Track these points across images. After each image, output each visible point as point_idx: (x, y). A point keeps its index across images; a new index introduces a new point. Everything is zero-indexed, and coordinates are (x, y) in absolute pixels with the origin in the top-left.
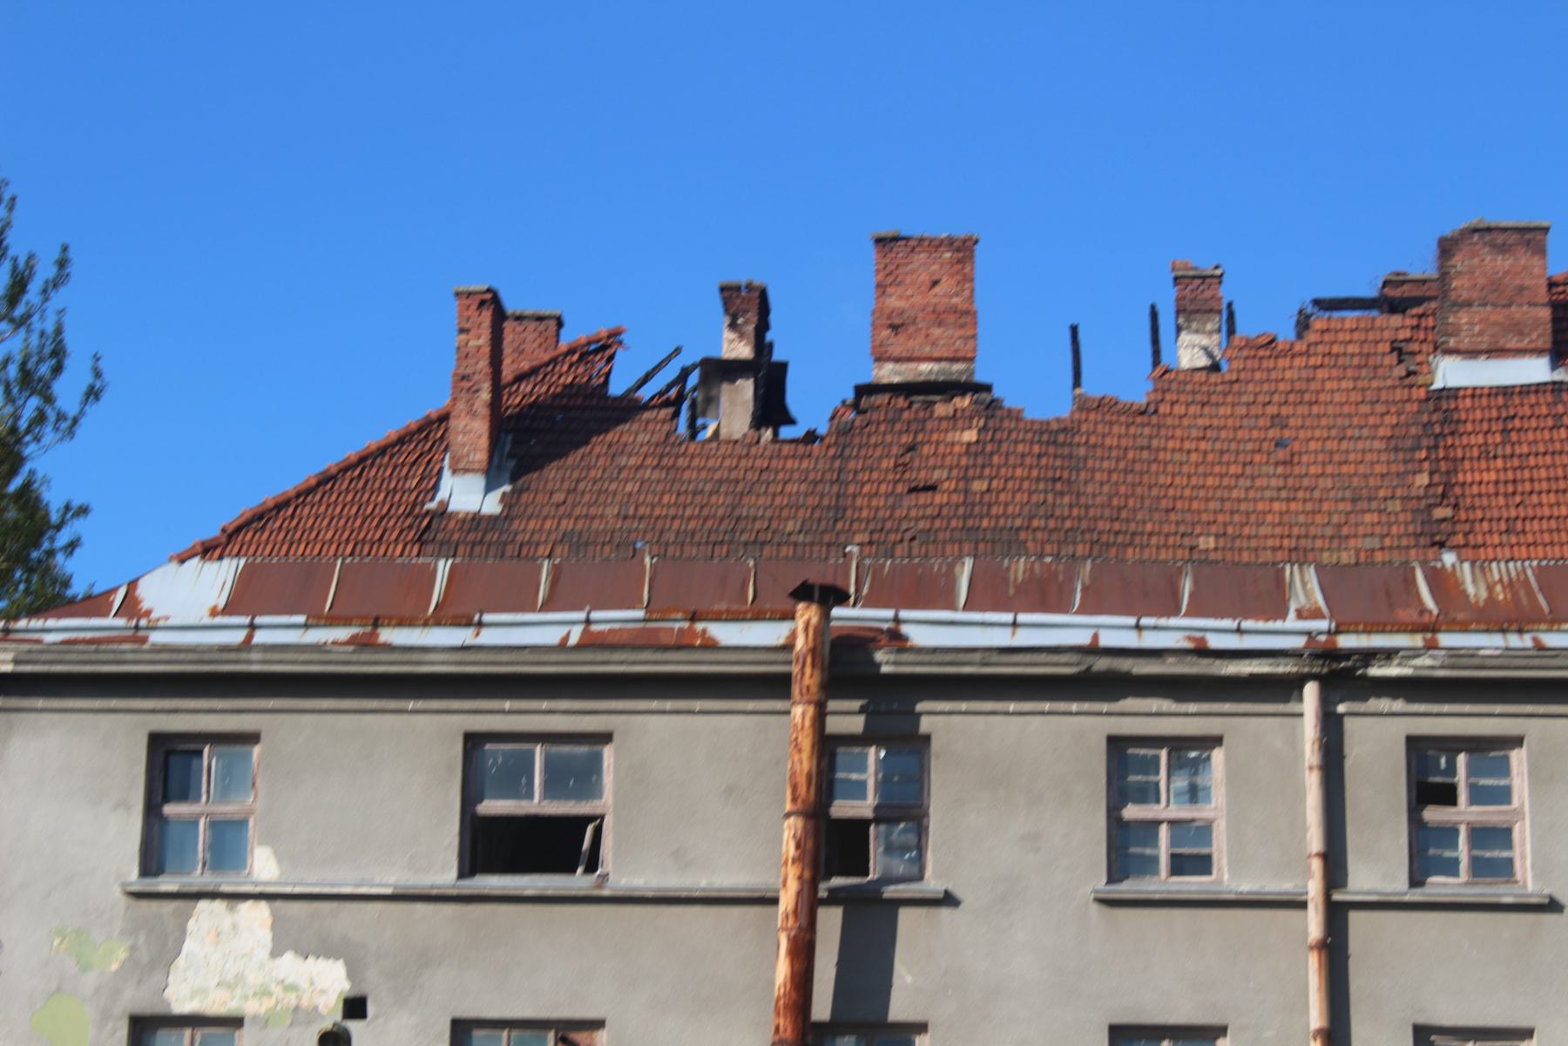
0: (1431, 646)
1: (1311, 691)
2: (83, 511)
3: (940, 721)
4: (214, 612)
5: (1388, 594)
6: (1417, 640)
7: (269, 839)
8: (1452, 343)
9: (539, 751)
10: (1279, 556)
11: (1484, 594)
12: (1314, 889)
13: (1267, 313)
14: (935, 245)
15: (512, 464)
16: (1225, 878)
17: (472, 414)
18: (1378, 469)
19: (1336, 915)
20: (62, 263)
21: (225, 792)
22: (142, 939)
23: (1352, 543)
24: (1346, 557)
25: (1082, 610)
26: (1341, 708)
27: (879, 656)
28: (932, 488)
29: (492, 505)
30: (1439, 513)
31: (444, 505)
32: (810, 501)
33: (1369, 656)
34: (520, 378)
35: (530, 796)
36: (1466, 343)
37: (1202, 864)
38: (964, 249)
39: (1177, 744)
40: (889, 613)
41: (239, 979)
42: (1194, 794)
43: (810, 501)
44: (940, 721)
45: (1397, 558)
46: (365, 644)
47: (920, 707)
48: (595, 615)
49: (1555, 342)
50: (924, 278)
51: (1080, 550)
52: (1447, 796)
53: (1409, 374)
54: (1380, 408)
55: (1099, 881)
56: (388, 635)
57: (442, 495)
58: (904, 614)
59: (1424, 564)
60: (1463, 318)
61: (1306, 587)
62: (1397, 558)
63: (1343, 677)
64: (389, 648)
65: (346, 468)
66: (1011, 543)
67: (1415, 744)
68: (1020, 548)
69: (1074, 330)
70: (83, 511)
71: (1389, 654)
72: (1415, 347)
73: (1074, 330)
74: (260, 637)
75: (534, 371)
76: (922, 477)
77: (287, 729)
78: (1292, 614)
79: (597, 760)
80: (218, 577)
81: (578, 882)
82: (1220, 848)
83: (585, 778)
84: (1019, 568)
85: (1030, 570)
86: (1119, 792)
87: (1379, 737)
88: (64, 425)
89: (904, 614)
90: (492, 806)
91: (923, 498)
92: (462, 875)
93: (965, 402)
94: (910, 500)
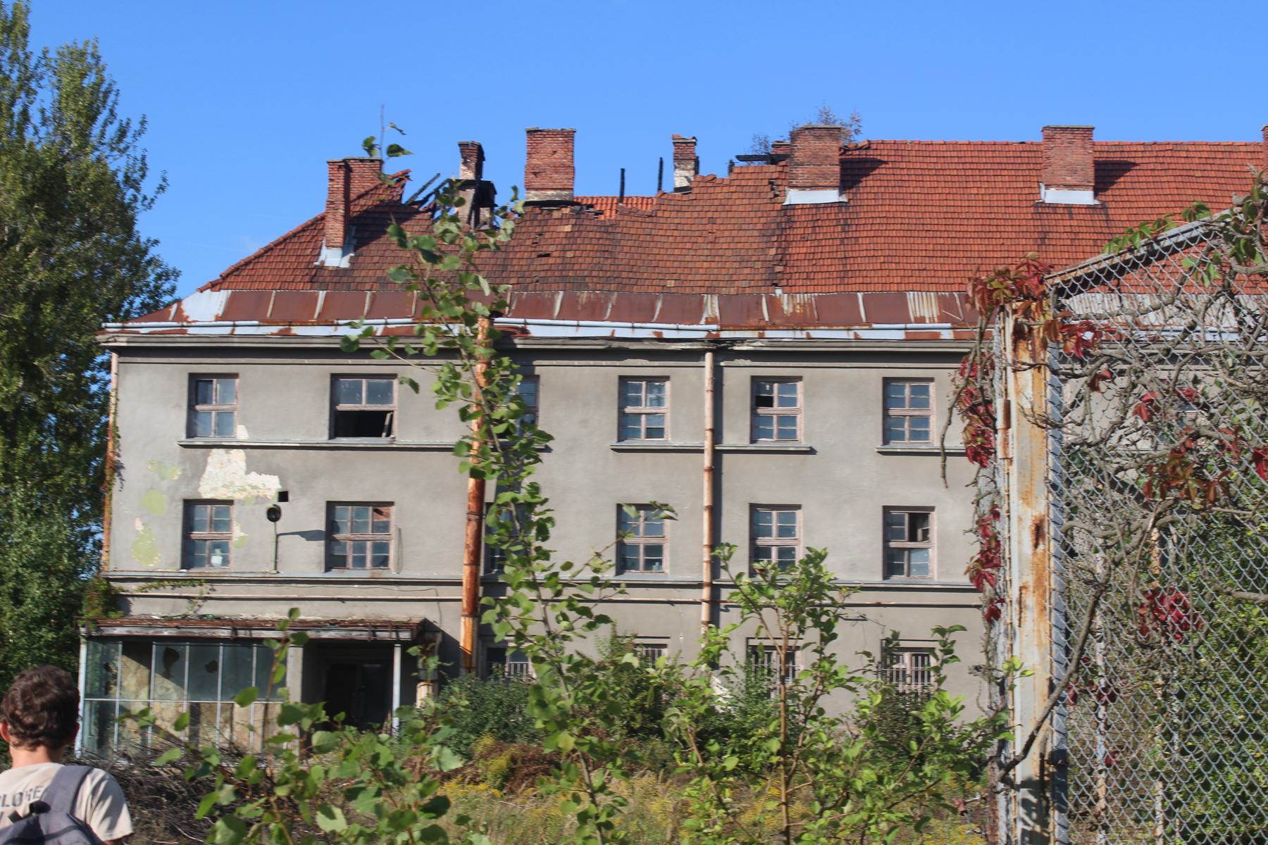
0: (761, 337)
1: (709, 356)
2: (156, 242)
3: (544, 369)
4: (218, 318)
5: (749, 310)
6: (755, 334)
7: (244, 422)
8: (794, 183)
9: (364, 381)
10: (703, 290)
11: (791, 310)
12: (707, 445)
13: (714, 164)
14: (554, 134)
15: (354, 242)
16: (670, 440)
17: (336, 220)
18: (755, 246)
19: (717, 456)
20: (143, 123)
21: (223, 401)
22: (188, 466)
23: (737, 284)
24: (733, 291)
25: (611, 319)
26: (722, 364)
27: (516, 341)
28: (548, 255)
29: (344, 263)
30: (779, 269)
31: (323, 262)
32: (492, 261)
33: (734, 341)
34: (360, 197)
35: (360, 402)
36: (800, 183)
37: (659, 432)
38: (569, 136)
39: (650, 379)
40: (522, 320)
41: (232, 483)
42: (659, 401)
43: (492, 261)
44: (544, 369)
45: (755, 291)
46: (285, 334)
47: (535, 363)
48: (390, 321)
49: (842, 181)
50: (550, 150)
51: (613, 287)
52: (768, 402)
53: (776, 196)
54: (759, 214)
55: (614, 441)
56: (296, 330)
57: (322, 258)
58: (529, 321)
59: (767, 294)
60: (800, 171)
61: (712, 307)
62: (755, 291)
63: (723, 350)
64: (296, 336)
65: (277, 244)
66: (581, 283)
67: (754, 379)
68: (586, 286)
69: (623, 171)
70: (156, 242)
71: (742, 341)
72: (779, 182)
73: (623, 171)
74: (238, 331)
75: (367, 193)
76: (544, 249)
77: (252, 373)
78: (703, 321)
79: (391, 385)
80: (218, 300)
81: (382, 441)
82: (667, 426)
83: (386, 394)
84: (584, 296)
85: (589, 298)
86: (623, 400)
87: (738, 377)
88: (146, 202)
89: (529, 321)
90: (343, 407)
91: (544, 260)
92: (331, 437)
93: (567, 211)
94: (537, 262)
